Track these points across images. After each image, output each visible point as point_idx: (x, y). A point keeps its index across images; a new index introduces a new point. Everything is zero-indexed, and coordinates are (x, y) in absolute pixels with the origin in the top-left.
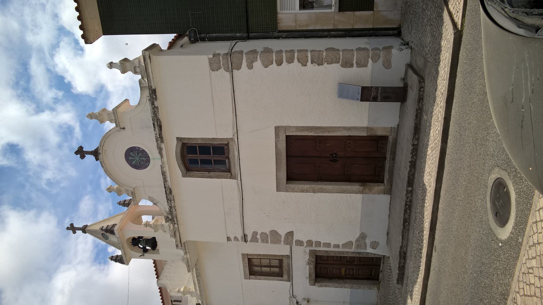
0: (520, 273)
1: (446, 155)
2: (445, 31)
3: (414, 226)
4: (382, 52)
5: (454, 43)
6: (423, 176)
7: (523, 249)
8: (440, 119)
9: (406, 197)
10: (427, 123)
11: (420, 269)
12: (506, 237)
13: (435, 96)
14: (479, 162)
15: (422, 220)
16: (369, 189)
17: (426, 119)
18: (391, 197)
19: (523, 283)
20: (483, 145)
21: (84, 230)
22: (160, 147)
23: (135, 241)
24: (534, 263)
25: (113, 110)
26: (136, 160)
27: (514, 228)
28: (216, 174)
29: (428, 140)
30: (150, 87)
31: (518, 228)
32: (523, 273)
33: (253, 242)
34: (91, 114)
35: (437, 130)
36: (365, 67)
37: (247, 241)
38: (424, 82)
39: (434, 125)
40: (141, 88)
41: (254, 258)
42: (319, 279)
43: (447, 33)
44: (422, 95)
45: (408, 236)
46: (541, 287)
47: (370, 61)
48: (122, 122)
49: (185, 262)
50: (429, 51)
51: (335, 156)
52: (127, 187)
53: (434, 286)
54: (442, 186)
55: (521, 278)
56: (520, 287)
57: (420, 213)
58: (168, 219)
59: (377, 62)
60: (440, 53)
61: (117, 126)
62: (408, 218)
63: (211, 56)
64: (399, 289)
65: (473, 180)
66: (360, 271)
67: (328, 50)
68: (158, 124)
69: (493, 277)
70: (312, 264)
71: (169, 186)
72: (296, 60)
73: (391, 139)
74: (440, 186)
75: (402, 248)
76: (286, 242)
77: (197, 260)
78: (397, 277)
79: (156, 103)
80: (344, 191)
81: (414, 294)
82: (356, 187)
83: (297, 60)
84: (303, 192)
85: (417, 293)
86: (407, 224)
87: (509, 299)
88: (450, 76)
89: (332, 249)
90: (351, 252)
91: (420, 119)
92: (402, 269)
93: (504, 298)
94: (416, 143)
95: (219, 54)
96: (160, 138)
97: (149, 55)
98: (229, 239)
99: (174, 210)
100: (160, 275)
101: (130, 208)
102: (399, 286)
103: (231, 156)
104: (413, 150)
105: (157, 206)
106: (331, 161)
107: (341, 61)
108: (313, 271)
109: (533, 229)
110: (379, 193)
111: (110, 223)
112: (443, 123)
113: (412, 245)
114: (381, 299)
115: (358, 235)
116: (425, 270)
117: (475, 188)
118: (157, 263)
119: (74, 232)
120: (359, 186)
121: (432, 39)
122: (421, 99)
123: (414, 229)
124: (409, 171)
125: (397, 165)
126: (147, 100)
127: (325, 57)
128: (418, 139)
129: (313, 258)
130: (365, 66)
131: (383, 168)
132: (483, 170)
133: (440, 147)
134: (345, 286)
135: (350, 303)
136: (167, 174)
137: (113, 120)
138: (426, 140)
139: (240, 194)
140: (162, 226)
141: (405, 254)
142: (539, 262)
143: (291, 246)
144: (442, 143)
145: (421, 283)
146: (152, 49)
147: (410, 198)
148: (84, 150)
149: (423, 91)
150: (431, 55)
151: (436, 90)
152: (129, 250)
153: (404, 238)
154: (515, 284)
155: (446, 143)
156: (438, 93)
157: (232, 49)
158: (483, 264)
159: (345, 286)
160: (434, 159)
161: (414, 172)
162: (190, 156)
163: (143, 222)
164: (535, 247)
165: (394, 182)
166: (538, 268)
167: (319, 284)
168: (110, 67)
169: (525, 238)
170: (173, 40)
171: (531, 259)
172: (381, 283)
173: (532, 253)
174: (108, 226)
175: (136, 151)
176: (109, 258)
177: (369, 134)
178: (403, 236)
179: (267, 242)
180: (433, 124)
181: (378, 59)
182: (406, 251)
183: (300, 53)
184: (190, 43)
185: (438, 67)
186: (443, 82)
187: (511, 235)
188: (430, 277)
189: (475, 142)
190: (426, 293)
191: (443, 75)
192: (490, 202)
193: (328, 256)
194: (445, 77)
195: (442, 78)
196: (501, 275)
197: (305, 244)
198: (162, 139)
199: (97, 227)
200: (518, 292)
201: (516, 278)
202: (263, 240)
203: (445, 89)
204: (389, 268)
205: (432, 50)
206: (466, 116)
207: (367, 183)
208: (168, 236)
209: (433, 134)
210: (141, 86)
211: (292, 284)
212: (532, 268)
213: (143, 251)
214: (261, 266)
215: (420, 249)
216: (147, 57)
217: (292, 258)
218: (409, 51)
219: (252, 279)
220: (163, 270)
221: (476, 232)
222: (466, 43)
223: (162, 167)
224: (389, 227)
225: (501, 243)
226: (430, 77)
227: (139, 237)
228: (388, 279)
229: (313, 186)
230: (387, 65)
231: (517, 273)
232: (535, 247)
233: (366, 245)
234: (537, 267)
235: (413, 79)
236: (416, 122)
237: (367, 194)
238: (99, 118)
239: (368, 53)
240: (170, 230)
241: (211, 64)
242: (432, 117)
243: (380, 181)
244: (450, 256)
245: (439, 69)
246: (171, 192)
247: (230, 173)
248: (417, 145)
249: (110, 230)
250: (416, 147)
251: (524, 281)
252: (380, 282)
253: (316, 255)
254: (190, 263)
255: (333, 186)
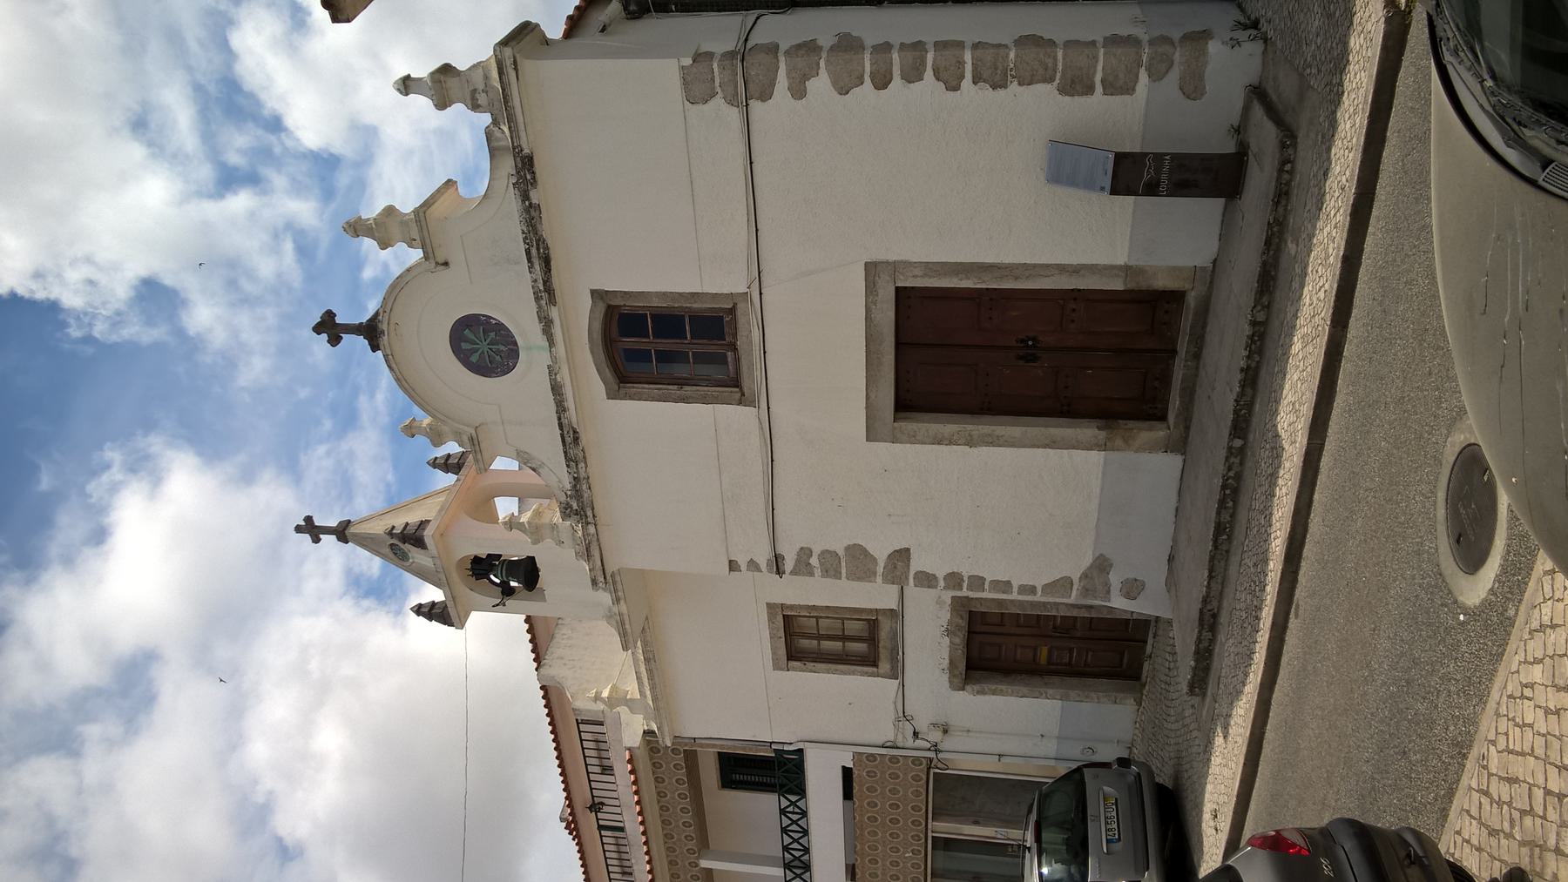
0: (1502, 694)
1: (1340, 361)
2: (1362, 7)
3: (1243, 544)
4: (1178, 49)
5: (1385, 48)
6: (1276, 413)
7: (1515, 631)
8: (1331, 259)
9: (1227, 465)
10: (1296, 266)
11: (1253, 659)
12: (1477, 602)
13: (1323, 190)
14: (1426, 393)
15: (1266, 531)
16: (1123, 437)
17: (1293, 252)
18: (1184, 461)
19: (1508, 720)
20: (1439, 348)
21: (342, 533)
22: (545, 318)
23: (481, 567)
24: (1536, 674)
25: (416, 211)
26: (481, 350)
27: (1498, 579)
28: (698, 390)
29: (1297, 314)
30: (517, 150)
31: (1508, 581)
32: (1510, 697)
33: (800, 575)
34: (356, 222)
35: (1323, 290)
36: (1129, 94)
37: (784, 573)
38: (1295, 145)
39: (1314, 272)
40: (493, 152)
41: (800, 616)
42: (978, 674)
43: (1367, 14)
44: (1285, 184)
45: (1226, 570)
46: (1549, 733)
47: (1143, 77)
48: (440, 246)
49: (614, 623)
50: (1314, 57)
51: (1034, 346)
52: (457, 425)
53: (1287, 705)
54: (1326, 443)
55: (1505, 708)
56: (1499, 731)
57: (1262, 512)
58: (569, 510)
59: (1162, 79)
60: (1344, 69)
61: (426, 257)
62: (1228, 522)
63: (688, 61)
64: (1193, 706)
65: (1406, 441)
66: (1090, 654)
67: (1023, 41)
68: (540, 254)
69: (1438, 697)
70: (959, 633)
71: (570, 424)
72: (929, 74)
73: (1192, 300)
74: (1319, 442)
75: (1208, 600)
76: (889, 577)
77: (647, 618)
78: (1189, 677)
79: (535, 196)
80: (1054, 442)
81: (1232, 723)
82: (1088, 431)
83: (932, 73)
84: (939, 444)
85: (1240, 721)
86: (1225, 537)
87: (1470, 756)
88: (1366, 139)
89: (1015, 596)
90: (1066, 605)
91: (1278, 250)
92: (1204, 656)
93: (1460, 753)
94: (1261, 317)
95: (710, 55)
96: (546, 292)
97: (514, 57)
98: (733, 566)
99: (584, 487)
100: (546, 654)
101: (463, 478)
102: (1196, 700)
103: (741, 343)
104: (1251, 337)
105: (539, 474)
106: (1021, 358)
107: (1058, 76)
108: (960, 651)
109: (1543, 589)
110: (1152, 448)
111: (413, 518)
112: (1338, 273)
113: (1236, 594)
114: (1143, 730)
115: (1087, 561)
116: (1265, 664)
117: (1410, 464)
118: (539, 628)
119: (316, 540)
120: (1096, 430)
121: (1324, 23)
122: (1282, 194)
123: (1243, 552)
124: (1238, 396)
125: (1206, 373)
126: (507, 187)
127: (1012, 65)
128: (1268, 307)
129: (962, 618)
130: (1129, 89)
131: (1166, 380)
132: (1435, 417)
133: (1326, 337)
134: (1046, 693)
135: (1058, 738)
136: (567, 393)
137: (415, 240)
138: (1290, 310)
139: (766, 445)
140: (553, 527)
141: (1215, 616)
142: (1549, 673)
143: (902, 587)
144: (1333, 327)
145: (1253, 697)
146: (522, 39)
147: (1236, 468)
148: (337, 322)
149: (1291, 172)
150: (1319, 71)
151: (1326, 174)
152: (462, 590)
153: (1213, 574)
154: (1489, 721)
155: (1345, 326)
156: (1332, 184)
157: (746, 40)
158: (1416, 662)
159: (1046, 693)
160: (1309, 369)
161: (1254, 397)
162: (630, 342)
163: (500, 518)
164: (1544, 633)
165: (1194, 421)
166: (1547, 686)
167: (977, 687)
168: (402, 89)
169: (1522, 608)
170: (577, 8)
171: (1532, 664)
172: (1147, 687)
173: (1535, 648)
174: (407, 524)
175: (481, 328)
176: (411, 609)
177: (1131, 286)
178: (1211, 571)
179: (837, 576)
180: (1312, 271)
181: (1167, 71)
182: (1218, 611)
183: (943, 53)
184: (627, 19)
185: (1336, 108)
186: (1346, 154)
187: (1492, 597)
188: (1279, 681)
189: (1419, 338)
190: (1265, 723)
191: (1349, 134)
192: (1444, 504)
193: (1002, 613)
194: (1354, 140)
195: (1345, 142)
196: (1458, 695)
197: (942, 583)
198: (552, 294)
199: (379, 528)
200: (1494, 743)
201: (1491, 705)
202: (827, 572)
203: (1350, 176)
204: (1169, 649)
205: (1323, 56)
206: (1402, 261)
207: (1120, 421)
208: (568, 553)
209: (1310, 299)
210: (492, 144)
211: (903, 686)
212: (1531, 686)
213: (503, 593)
214: (820, 637)
215: (1256, 607)
216: (509, 62)
217: (903, 617)
218: (1258, 47)
219: (794, 669)
220: (554, 641)
221: (1405, 578)
222: (1417, 51)
223: (552, 371)
224: (1175, 540)
225: (1465, 615)
226: (1312, 135)
227: (489, 555)
228: (1164, 678)
229: (969, 427)
230: (1193, 88)
231: (1495, 695)
232: (1544, 633)
233: (1109, 588)
234: (1543, 685)
235: (1264, 135)
236: (1265, 257)
237: (1118, 450)
238: (376, 234)
239: (1137, 53)
240: (574, 539)
241: (686, 83)
242: (1311, 251)
243: (1157, 415)
244: (1333, 635)
245: (1339, 114)
246: (576, 440)
247: (737, 390)
248: (1265, 323)
249: (412, 537)
250: (1262, 329)
251: (1510, 716)
252: (1145, 685)
253: (970, 612)
254: (627, 626)
255: (1024, 429)
